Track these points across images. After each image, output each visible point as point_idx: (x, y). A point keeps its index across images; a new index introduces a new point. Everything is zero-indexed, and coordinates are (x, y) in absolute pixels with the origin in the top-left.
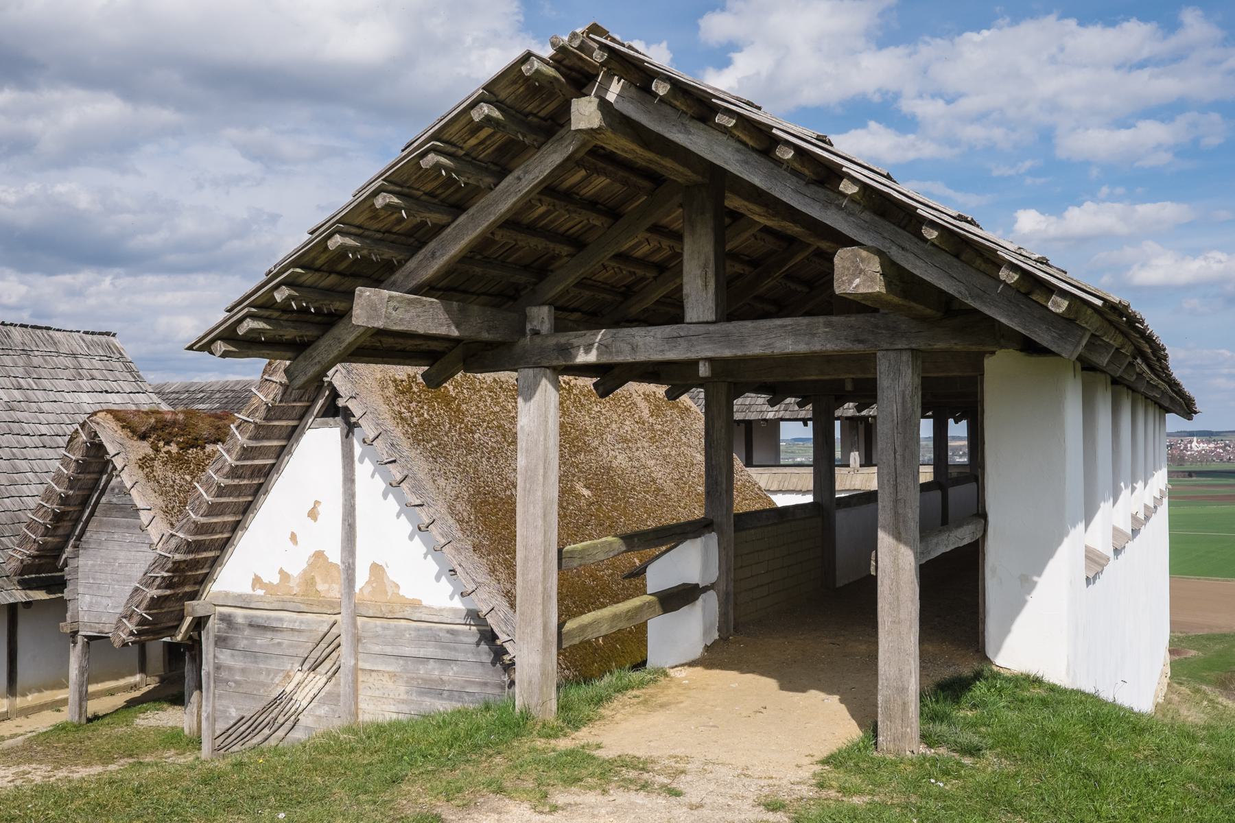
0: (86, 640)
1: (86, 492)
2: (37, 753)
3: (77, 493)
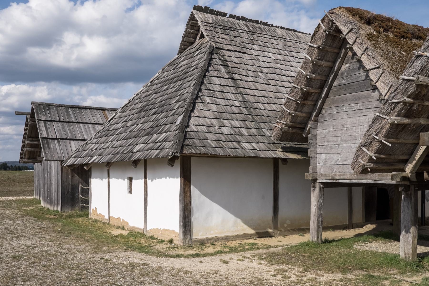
0: (321, 186)
1: (323, 78)
2: (291, 258)
3: (318, 77)
